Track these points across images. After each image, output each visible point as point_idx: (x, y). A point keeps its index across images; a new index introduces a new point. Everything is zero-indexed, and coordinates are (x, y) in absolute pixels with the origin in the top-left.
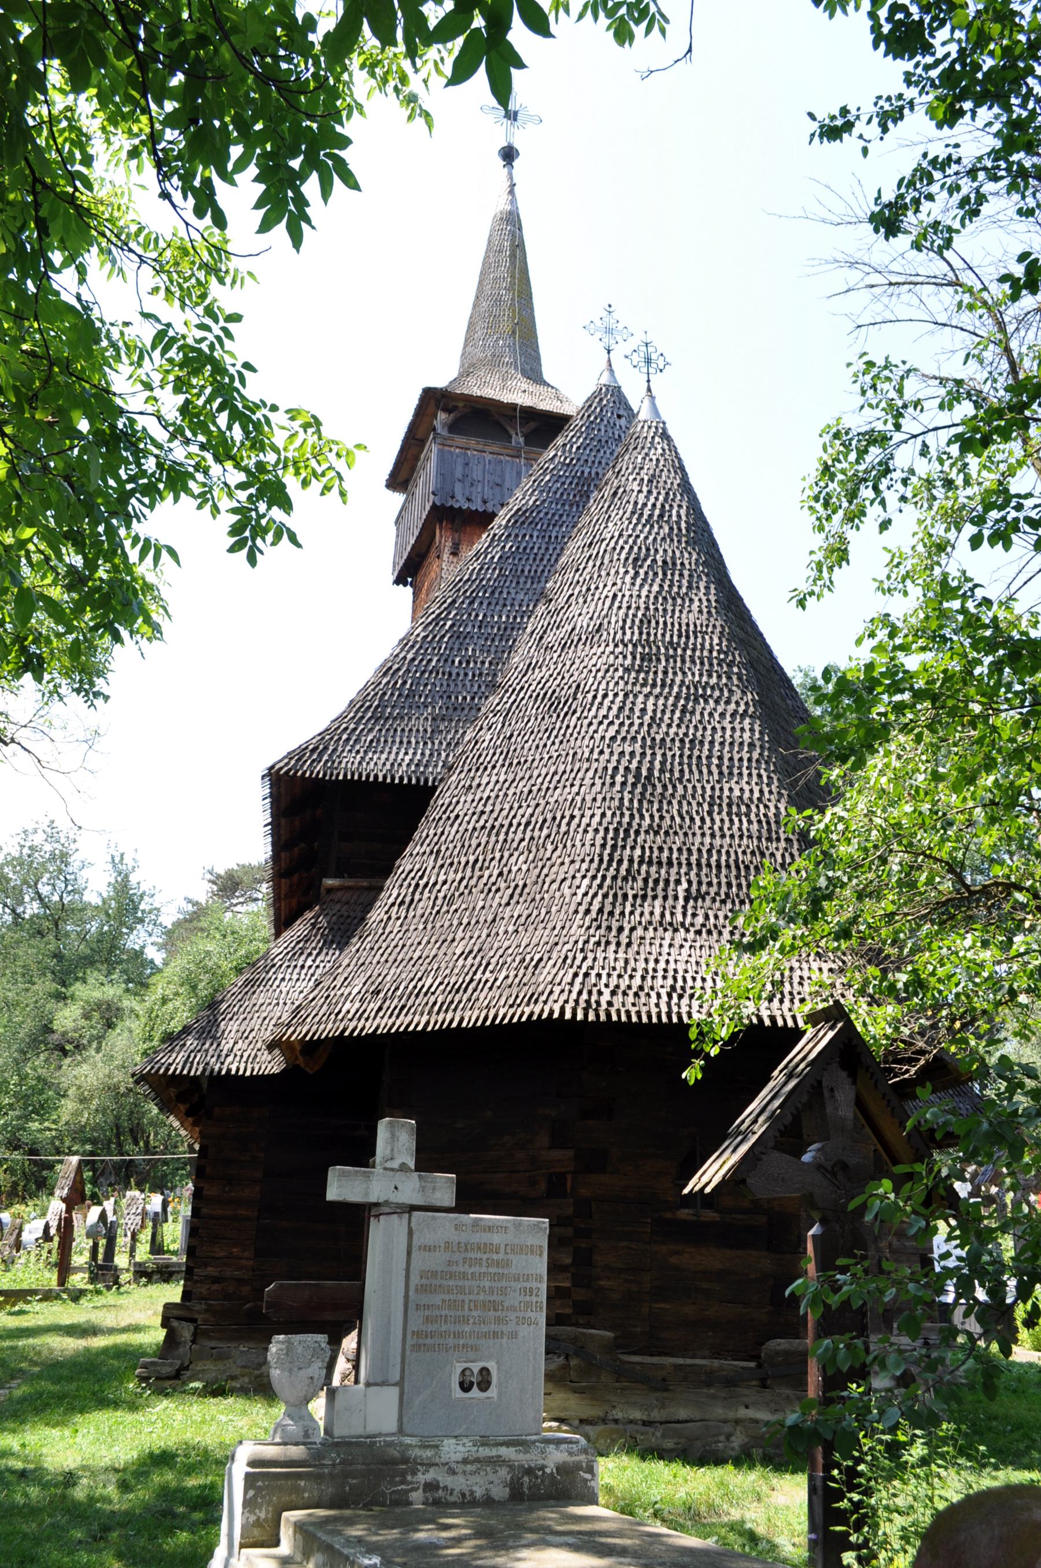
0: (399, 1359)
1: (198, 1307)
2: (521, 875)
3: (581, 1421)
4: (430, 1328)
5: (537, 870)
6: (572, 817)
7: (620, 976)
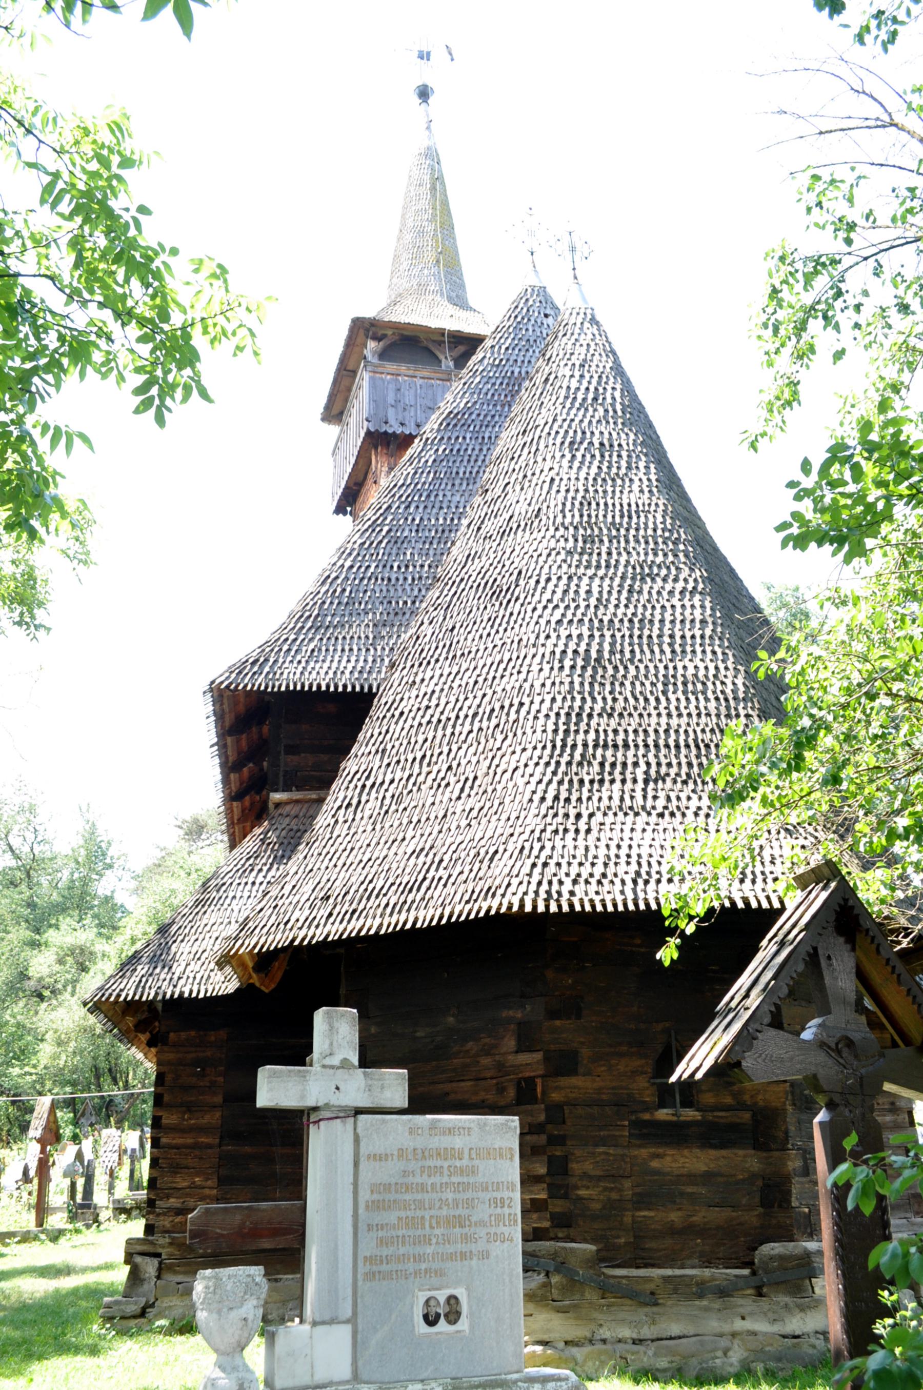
0: (349, 1291)
1: (161, 1241)
2: (469, 769)
3: (566, 1343)
4: (385, 1252)
5: (488, 761)
6: (521, 704)
7: (581, 864)
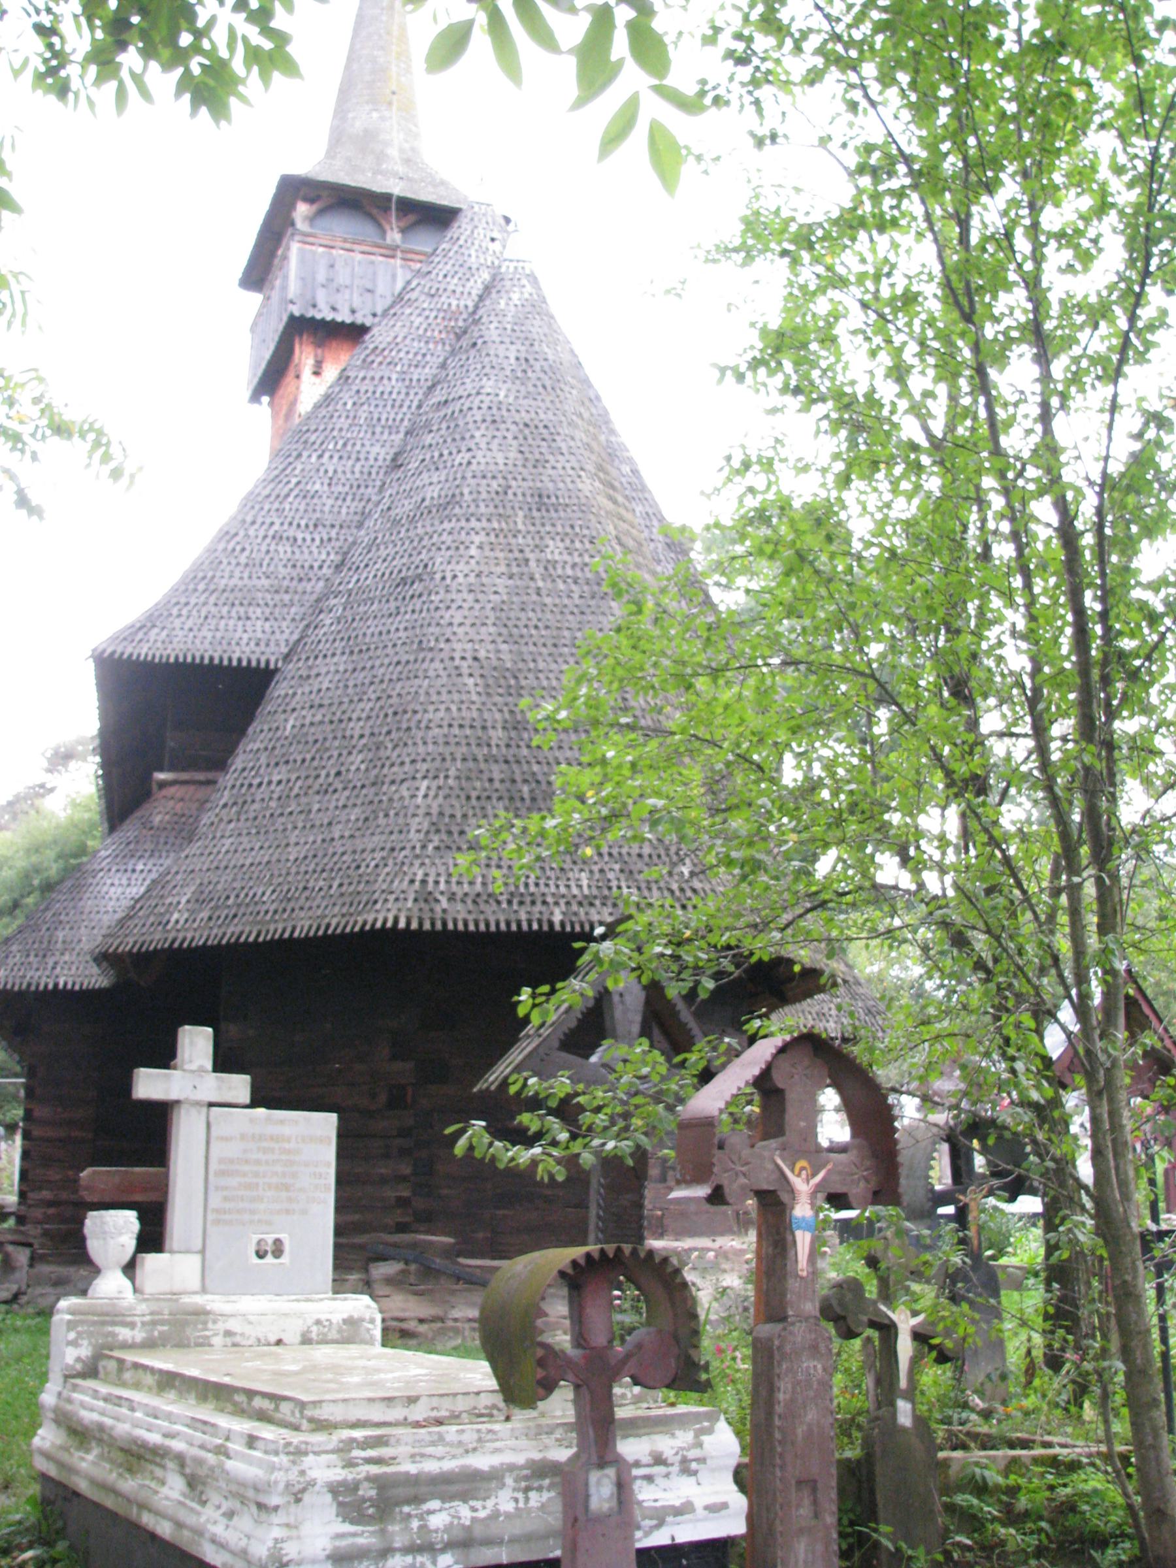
4: (228, 1205)
